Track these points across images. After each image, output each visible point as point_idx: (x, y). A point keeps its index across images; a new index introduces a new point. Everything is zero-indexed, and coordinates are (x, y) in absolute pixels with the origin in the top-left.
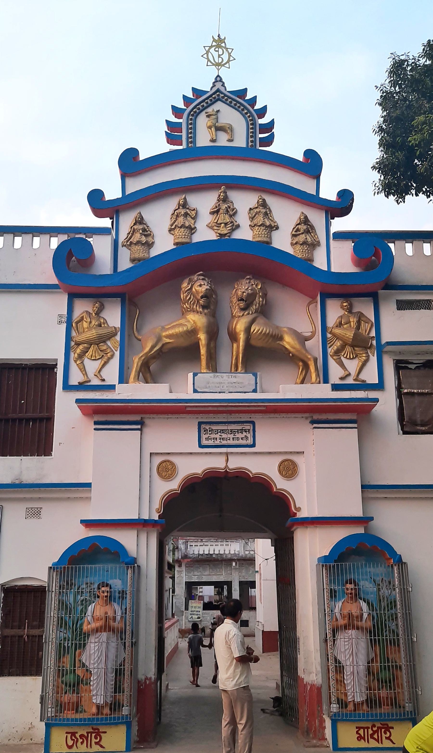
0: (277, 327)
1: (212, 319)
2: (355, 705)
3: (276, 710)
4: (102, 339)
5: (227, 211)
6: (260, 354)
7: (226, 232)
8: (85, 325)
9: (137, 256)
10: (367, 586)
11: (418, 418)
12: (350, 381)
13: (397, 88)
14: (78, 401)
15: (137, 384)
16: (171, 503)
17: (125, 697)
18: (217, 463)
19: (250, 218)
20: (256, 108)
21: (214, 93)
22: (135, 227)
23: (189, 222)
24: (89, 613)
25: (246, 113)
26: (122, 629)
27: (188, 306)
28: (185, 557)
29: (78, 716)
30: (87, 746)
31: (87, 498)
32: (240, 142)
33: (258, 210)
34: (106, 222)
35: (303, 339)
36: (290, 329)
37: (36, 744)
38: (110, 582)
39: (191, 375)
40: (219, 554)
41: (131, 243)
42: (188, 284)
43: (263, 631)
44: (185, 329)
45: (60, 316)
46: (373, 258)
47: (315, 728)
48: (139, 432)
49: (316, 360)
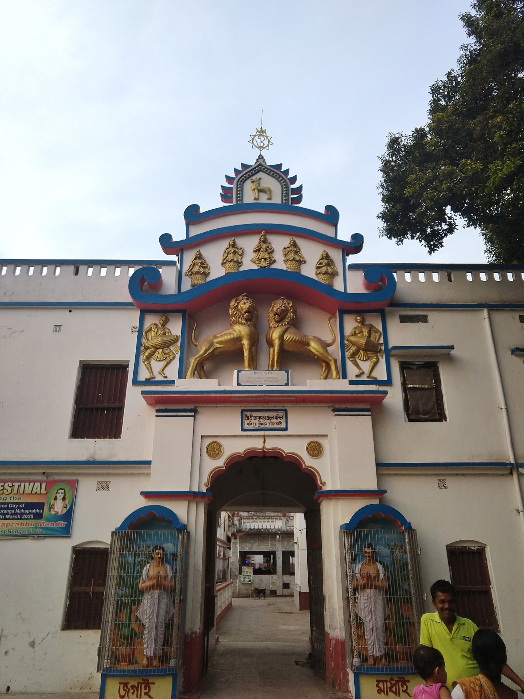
0: (305, 336)
1: (253, 329)
2: (374, 659)
3: (307, 663)
4: (166, 345)
5: (267, 250)
6: (293, 356)
7: (265, 265)
8: (153, 334)
9: (196, 282)
10: (383, 550)
11: (421, 408)
12: (364, 378)
13: (394, 158)
14: (143, 392)
15: (193, 379)
16: (218, 479)
17: (173, 650)
18: (257, 444)
19: (284, 254)
20: (288, 177)
21: (257, 166)
22: (195, 261)
23: (237, 258)
24: (144, 572)
25: (281, 180)
26: (171, 587)
27: (235, 319)
28: (240, 531)
29: (132, 667)
30: (137, 697)
31: (148, 474)
32: (277, 199)
33: (290, 249)
34: (174, 258)
35: (325, 345)
36: (314, 337)
37: (94, 693)
38: (164, 546)
39: (236, 372)
40: (266, 529)
41: (192, 273)
42: (235, 302)
43: (300, 592)
44: (232, 336)
45: (134, 327)
46: (380, 283)
47: (340, 680)
48: (192, 418)
49: (336, 361)
